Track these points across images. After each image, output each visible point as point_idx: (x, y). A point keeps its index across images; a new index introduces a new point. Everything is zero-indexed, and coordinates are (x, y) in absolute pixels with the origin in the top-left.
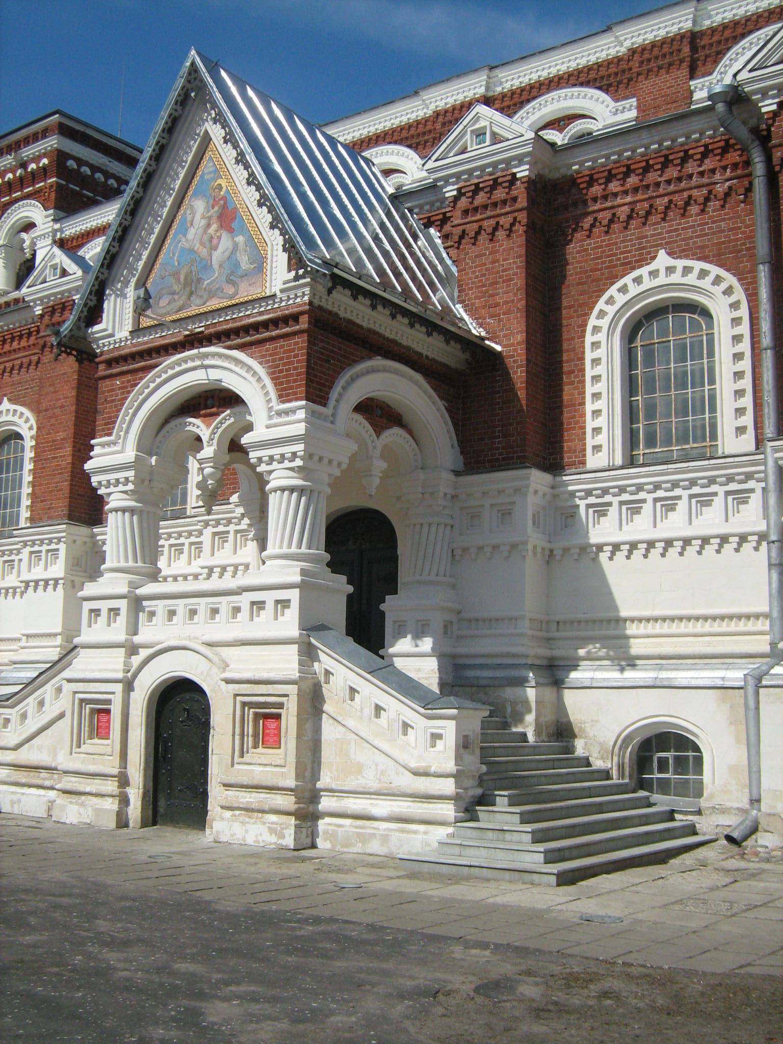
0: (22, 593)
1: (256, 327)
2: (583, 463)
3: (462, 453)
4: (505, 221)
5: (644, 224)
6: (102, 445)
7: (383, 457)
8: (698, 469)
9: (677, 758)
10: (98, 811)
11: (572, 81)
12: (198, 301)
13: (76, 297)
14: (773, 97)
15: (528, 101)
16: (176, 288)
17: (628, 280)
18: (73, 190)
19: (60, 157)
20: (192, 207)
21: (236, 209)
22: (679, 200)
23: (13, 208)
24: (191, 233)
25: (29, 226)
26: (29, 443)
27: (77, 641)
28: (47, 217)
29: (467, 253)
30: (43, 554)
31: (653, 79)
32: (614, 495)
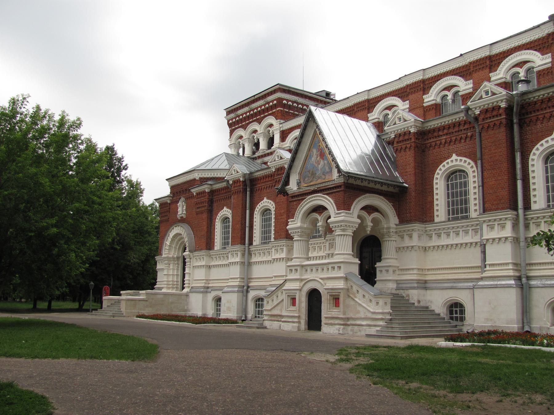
0: (273, 262)
1: (330, 189)
3: (398, 218)
4: (408, 146)
5: (449, 145)
6: (292, 221)
7: (372, 222)
8: (464, 222)
9: (460, 310)
10: (293, 327)
12: (315, 180)
14: (478, 109)
16: (310, 175)
17: (445, 163)
18: (286, 112)
20: (313, 151)
21: (324, 153)
22: (458, 138)
23: (265, 119)
24: (313, 159)
25: (271, 125)
26: (273, 213)
28: (277, 122)
29: (398, 155)
30: (279, 250)
31: (478, 73)
32: (451, 229)
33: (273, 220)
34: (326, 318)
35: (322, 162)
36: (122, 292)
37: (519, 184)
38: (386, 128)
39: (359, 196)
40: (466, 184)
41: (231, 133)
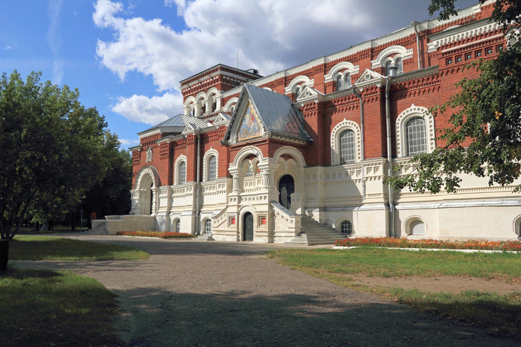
2: (331, 164)
6: (231, 165)
11: (345, 60)
13: (226, 125)
15: (334, 65)
17: (338, 125)
19: (221, 76)
21: (255, 117)
22: (348, 107)
24: (247, 121)
26: (217, 158)
27: (228, 205)
33: (217, 164)
34: (256, 232)
35: (253, 124)
36: (106, 217)
37: (388, 140)
38: (298, 100)
39: (279, 148)
40: (352, 139)
41: (185, 99)
